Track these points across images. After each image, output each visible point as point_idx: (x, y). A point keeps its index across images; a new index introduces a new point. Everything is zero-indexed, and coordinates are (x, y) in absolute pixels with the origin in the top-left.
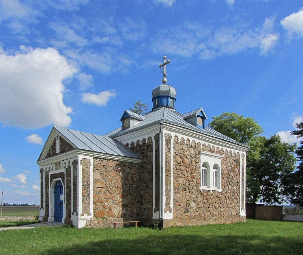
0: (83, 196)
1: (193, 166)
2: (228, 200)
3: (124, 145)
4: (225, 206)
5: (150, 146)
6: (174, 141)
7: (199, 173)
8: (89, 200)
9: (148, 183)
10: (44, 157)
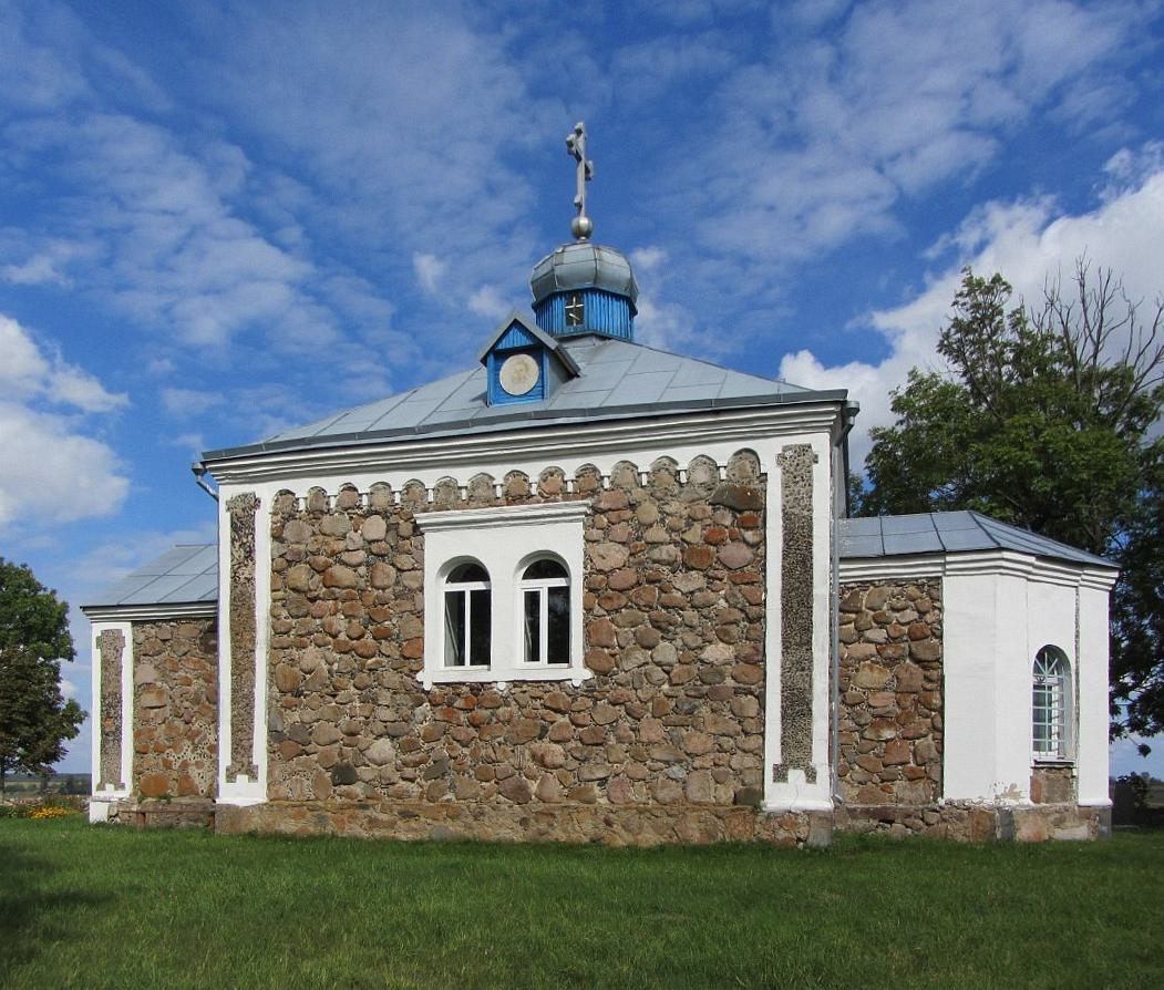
0: (104, 734)
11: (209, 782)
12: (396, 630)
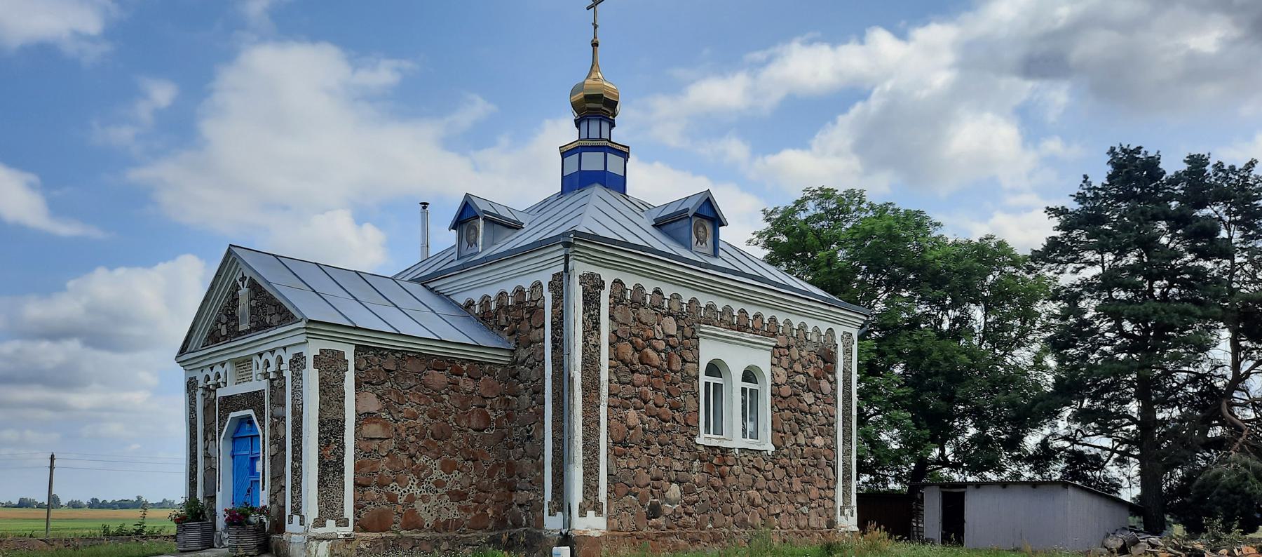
0: (323, 464)
1: (675, 372)
2: (795, 479)
3: (460, 306)
4: (784, 499)
5: (535, 310)
6: (610, 297)
7: (696, 395)
8: (343, 478)
9: (530, 425)
10: (198, 344)
11: (435, 516)
12: (683, 404)
